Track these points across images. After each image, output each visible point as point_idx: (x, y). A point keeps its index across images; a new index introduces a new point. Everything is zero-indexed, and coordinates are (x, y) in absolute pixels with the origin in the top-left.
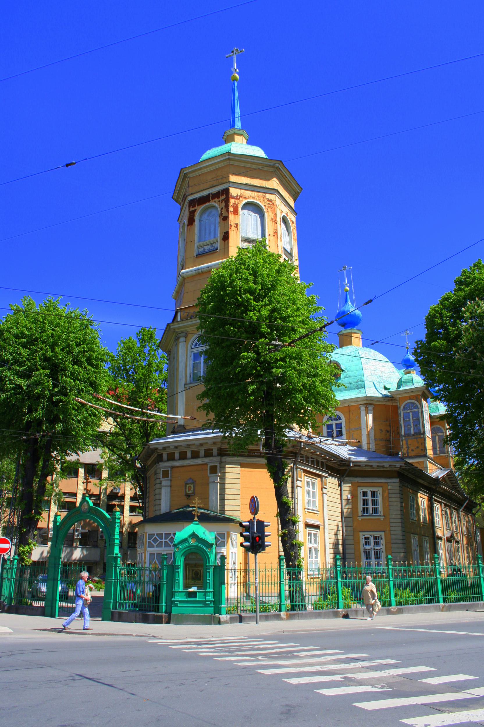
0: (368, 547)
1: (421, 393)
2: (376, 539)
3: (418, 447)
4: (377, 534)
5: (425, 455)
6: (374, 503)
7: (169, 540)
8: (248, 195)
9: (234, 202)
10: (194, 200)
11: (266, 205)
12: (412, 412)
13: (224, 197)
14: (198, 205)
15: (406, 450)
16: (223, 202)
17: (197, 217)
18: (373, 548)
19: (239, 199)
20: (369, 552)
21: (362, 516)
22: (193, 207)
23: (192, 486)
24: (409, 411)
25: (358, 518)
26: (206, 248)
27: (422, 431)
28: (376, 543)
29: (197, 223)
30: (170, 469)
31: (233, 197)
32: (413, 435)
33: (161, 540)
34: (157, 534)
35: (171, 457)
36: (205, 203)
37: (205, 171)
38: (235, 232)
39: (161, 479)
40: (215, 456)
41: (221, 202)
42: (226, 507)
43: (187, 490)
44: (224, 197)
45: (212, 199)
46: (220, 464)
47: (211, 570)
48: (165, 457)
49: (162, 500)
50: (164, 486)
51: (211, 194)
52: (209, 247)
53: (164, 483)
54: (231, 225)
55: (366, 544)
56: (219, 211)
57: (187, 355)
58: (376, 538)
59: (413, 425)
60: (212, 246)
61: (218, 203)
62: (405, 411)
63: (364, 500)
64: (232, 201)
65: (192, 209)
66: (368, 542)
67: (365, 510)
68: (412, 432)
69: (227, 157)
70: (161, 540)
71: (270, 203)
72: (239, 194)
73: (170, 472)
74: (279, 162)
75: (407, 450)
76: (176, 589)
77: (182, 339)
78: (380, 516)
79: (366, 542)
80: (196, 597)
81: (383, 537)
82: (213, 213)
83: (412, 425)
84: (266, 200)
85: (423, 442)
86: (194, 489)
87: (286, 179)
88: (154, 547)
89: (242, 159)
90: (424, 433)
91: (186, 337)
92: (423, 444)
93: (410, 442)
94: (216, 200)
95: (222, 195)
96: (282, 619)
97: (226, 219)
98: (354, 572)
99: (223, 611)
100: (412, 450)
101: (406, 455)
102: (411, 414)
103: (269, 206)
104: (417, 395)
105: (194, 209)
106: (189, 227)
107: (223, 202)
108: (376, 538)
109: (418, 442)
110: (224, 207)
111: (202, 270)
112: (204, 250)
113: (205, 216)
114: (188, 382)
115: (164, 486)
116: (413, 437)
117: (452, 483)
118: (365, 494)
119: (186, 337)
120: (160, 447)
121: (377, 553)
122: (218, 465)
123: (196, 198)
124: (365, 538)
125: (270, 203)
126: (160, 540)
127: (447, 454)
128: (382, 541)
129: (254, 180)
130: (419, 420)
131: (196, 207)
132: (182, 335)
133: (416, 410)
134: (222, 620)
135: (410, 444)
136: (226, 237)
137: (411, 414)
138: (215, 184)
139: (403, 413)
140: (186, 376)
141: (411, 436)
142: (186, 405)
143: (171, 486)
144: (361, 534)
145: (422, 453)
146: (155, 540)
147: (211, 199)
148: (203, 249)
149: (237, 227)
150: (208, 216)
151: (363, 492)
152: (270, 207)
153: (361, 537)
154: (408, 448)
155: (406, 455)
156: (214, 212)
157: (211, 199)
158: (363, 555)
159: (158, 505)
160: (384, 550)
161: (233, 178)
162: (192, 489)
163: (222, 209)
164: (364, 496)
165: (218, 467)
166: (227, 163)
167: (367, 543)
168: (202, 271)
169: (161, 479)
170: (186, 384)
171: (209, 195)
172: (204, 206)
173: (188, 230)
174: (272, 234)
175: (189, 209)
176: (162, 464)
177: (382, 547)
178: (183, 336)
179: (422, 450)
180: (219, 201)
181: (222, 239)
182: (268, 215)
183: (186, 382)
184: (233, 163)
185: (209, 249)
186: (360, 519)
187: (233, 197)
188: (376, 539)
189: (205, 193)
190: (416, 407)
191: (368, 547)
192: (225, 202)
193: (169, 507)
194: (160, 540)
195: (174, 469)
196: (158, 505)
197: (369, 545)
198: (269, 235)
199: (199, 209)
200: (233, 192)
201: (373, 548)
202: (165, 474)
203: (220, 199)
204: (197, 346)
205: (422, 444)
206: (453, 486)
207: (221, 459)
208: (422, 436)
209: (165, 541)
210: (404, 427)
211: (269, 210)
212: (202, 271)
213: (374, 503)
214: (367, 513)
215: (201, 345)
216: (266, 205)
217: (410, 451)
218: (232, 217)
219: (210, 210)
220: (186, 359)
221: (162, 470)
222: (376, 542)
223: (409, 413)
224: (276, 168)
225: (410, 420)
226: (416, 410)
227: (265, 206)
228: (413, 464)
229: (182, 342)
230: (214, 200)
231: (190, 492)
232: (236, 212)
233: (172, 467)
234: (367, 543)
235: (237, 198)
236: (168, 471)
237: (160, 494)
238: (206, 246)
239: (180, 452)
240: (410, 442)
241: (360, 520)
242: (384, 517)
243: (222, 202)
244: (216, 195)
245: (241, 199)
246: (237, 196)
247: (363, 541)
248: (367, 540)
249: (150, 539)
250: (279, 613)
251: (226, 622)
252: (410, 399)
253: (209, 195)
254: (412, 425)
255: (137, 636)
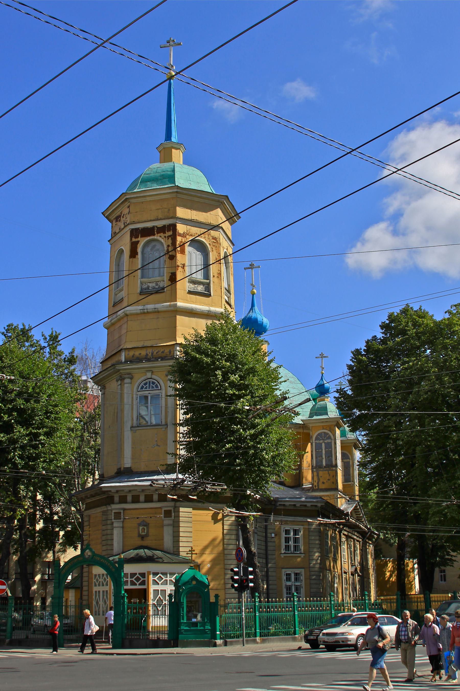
0: (289, 583)
1: (335, 423)
2: (296, 576)
3: (329, 480)
4: (297, 571)
5: (336, 489)
6: (296, 540)
7: (135, 579)
8: (194, 232)
9: (181, 240)
10: (137, 229)
11: (211, 243)
12: (325, 443)
13: (170, 233)
14: (141, 237)
15: (317, 482)
16: (170, 238)
17: (139, 250)
18: (293, 584)
19: (186, 237)
20: (290, 588)
21: (285, 553)
22: (135, 238)
23: (145, 528)
24: (321, 441)
25: (281, 555)
26: (150, 285)
27: (334, 463)
28: (296, 580)
29: (139, 256)
30: (122, 511)
31: (180, 235)
32: (325, 467)
33: (166, 579)
34: (139, 574)
35: (123, 500)
36: (149, 235)
37: (148, 199)
38: (182, 273)
39: (113, 520)
40: (170, 501)
41: (167, 238)
42: (181, 548)
43: (141, 532)
44: (170, 233)
45: (158, 233)
46: (174, 509)
47: (151, 605)
48: (116, 499)
49: (114, 540)
50: (115, 527)
51: (156, 227)
52: (154, 285)
53: (115, 525)
54: (178, 266)
55: (287, 581)
56: (166, 249)
57: (132, 398)
58: (296, 574)
59: (325, 456)
60: (157, 285)
61: (164, 238)
62: (318, 441)
63: (286, 538)
64: (179, 239)
65: (134, 240)
66: (289, 578)
67: (287, 548)
68: (324, 464)
69: (175, 190)
70: (131, 579)
71: (215, 241)
72: (186, 231)
73: (122, 514)
74: (225, 197)
75: (318, 483)
76: (182, 621)
77: (127, 381)
78: (301, 553)
79: (287, 578)
80: (197, 626)
81: (303, 574)
82: (157, 247)
83: (324, 456)
84: (211, 238)
85: (335, 474)
86: (148, 531)
87: (228, 211)
88: (136, 585)
89: (190, 193)
90: (336, 466)
91: (131, 378)
92: (335, 476)
93: (321, 473)
94: (162, 234)
95: (169, 231)
96: (257, 643)
97: (173, 258)
98: (317, 606)
99: (218, 637)
100: (323, 483)
101: (317, 488)
102: (323, 445)
103: (214, 244)
104: (331, 425)
105: (137, 240)
106: (131, 259)
107: (170, 238)
108: (296, 574)
109: (329, 475)
110: (170, 245)
111: (148, 310)
112: (148, 287)
113: (148, 249)
114: (135, 424)
115: (115, 527)
116: (325, 469)
117: (356, 514)
118: (287, 532)
119: (131, 378)
120: (113, 490)
121: (297, 589)
122: (172, 509)
123: (139, 228)
124: (287, 574)
125: (215, 241)
126: (133, 579)
127: (353, 483)
128: (302, 578)
129: (201, 213)
130: (331, 451)
131: (139, 239)
132: (127, 376)
133: (329, 441)
134: (218, 643)
135: (321, 477)
136: (173, 279)
137: (323, 445)
138: (160, 216)
139: (316, 443)
140: (132, 419)
141: (322, 468)
142: (132, 448)
143: (123, 527)
144: (283, 570)
145: (333, 487)
146: (138, 579)
147: (156, 233)
148: (146, 286)
149: (183, 268)
150: (151, 250)
151: (286, 530)
152: (214, 246)
153: (283, 573)
154: (319, 479)
155: (317, 488)
156: (158, 246)
157: (156, 233)
158: (285, 590)
159: (110, 545)
160: (303, 586)
161: (181, 212)
162: (146, 531)
163: (168, 246)
164: (286, 534)
165: (172, 511)
166: (174, 195)
167: (288, 579)
168: (147, 311)
169: (113, 520)
170: (132, 427)
171: (153, 227)
172: (149, 238)
173: (131, 263)
174: (216, 275)
175: (131, 239)
176: (114, 506)
177: (302, 583)
178: (128, 378)
179: (333, 483)
180: (165, 237)
181: (169, 280)
182: (213, 255)
183: (132, 424)
184: (179, 196)
185: (154, 287)
186: (282, 556)
187: (180, 235)
188: (296, 576)
189: (149, 225)
190: (329, 438)
191: (289, 583)
192: (172, 239)
193: (121, 548)
194: (133, 579)
195: (126, 511)
196: (110, 545)
197: (289, 581)
198: (214, 276)
199: (143, 241)
200: (181, 228)
201: (293, 584)
202: (118, 515)
203: (167, 235)
204: (144, 390)
205: (333, 477)
206: (357, 517)
207: (175, 504)
208: (334, 469)
209: (131, 581)
210: (316, 458)
211: (214, 248)
212: (147, 311)
213: (296, 540)
214: (288, 551)
215: (148, 389)
216: (211, 243)
217: (320, 483)
218: (179, 256)
219: (153, 244)
220: (132, 401)
221: (113, 511)
222: (296, 578)
223: (322, 443)
224: (222, 202)
225: (322, 451)
226: (329, 441)
227: (210, 244)
228: (323, 498)
229: (127, 383)
230: (159, 235)
231: (143, 534)
232: (183, 252)
233: (124, 509)
234: (288, 579)
235: (184, 235)
236: (121, 512)
237: (112, 534)
238: (150, 283)
239: (132, 495)
240: (321, 473)
241: (283, 557)
242: (304, 555)
243: (168, 239)
244: (162, 230)
245: (187, 237)
246: (184, 233)
247: (284, 578)
248: (288, 577)
249: (143, 580)
250: (255, 638)
251: (220, 645)
252: (323, 429)
253: (154, 227)
254: (324, 456)
255: (177, 653)
